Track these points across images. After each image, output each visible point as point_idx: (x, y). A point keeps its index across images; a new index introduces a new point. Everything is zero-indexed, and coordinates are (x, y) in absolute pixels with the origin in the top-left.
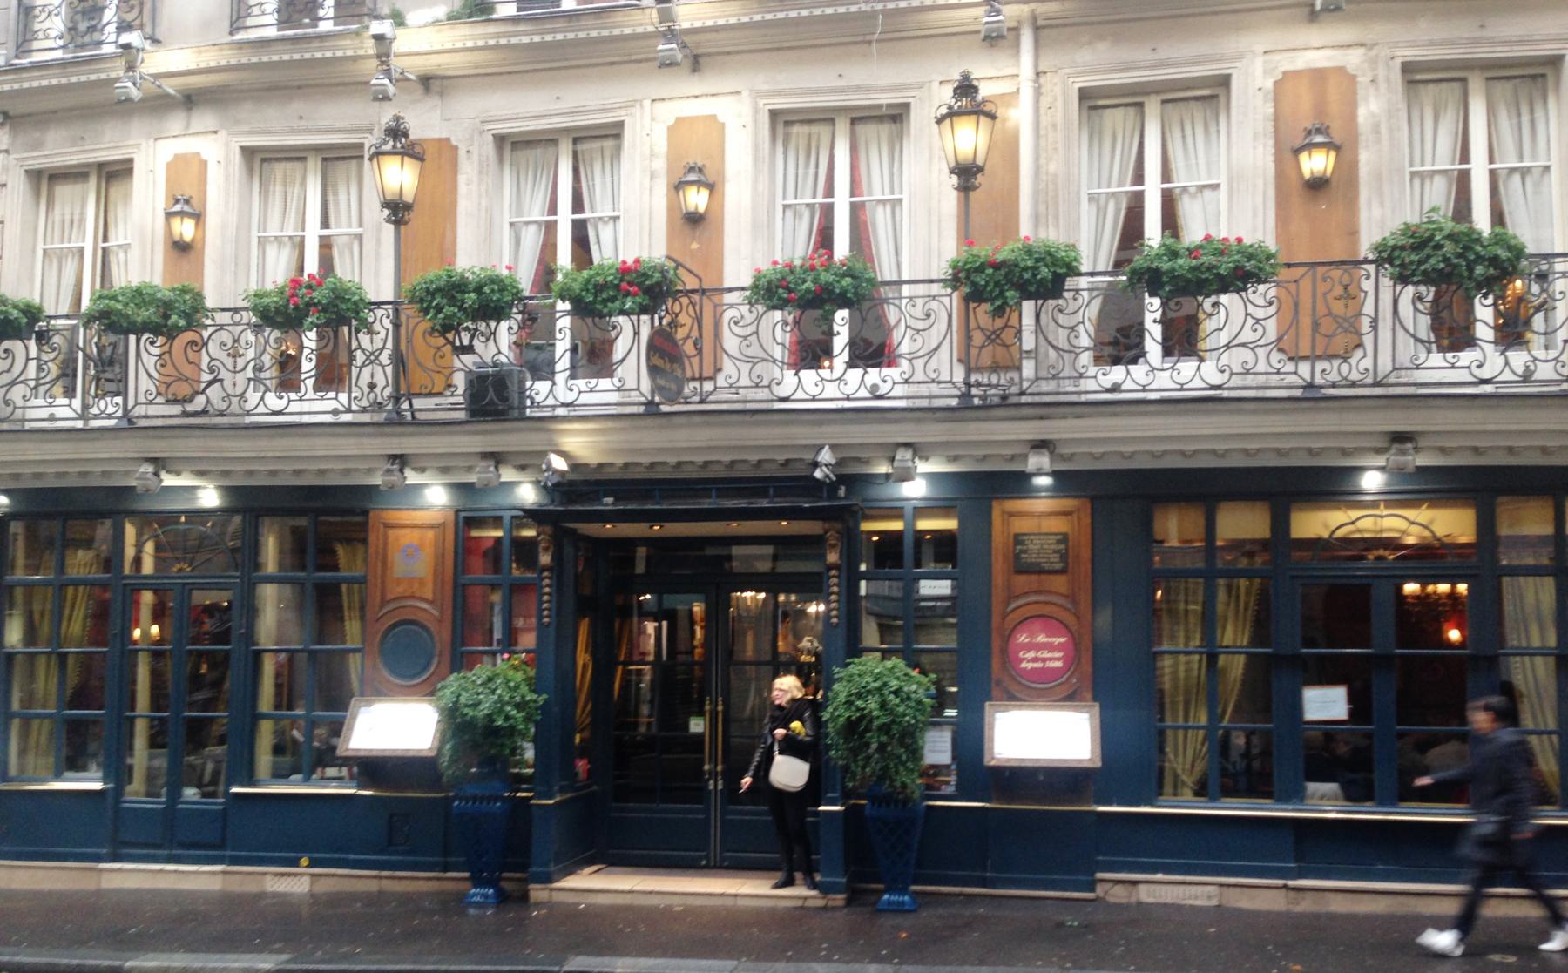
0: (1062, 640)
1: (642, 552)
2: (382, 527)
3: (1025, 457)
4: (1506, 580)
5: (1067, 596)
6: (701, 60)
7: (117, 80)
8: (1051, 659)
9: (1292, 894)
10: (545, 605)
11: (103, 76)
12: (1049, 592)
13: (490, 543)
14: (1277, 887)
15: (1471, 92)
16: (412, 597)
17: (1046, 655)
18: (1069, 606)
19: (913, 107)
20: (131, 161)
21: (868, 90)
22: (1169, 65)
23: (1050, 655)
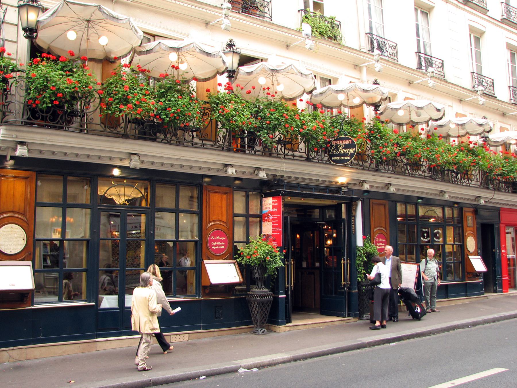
0: (224, 238)
2: (466, 274)
3: (15, 150)
7: (120, 113)
8: (221, 245)
10: (353, 226)
13: (449, 278)
15: (23, 209)
16: (219, 220)
17: (220, 244)
19: (339, 79)
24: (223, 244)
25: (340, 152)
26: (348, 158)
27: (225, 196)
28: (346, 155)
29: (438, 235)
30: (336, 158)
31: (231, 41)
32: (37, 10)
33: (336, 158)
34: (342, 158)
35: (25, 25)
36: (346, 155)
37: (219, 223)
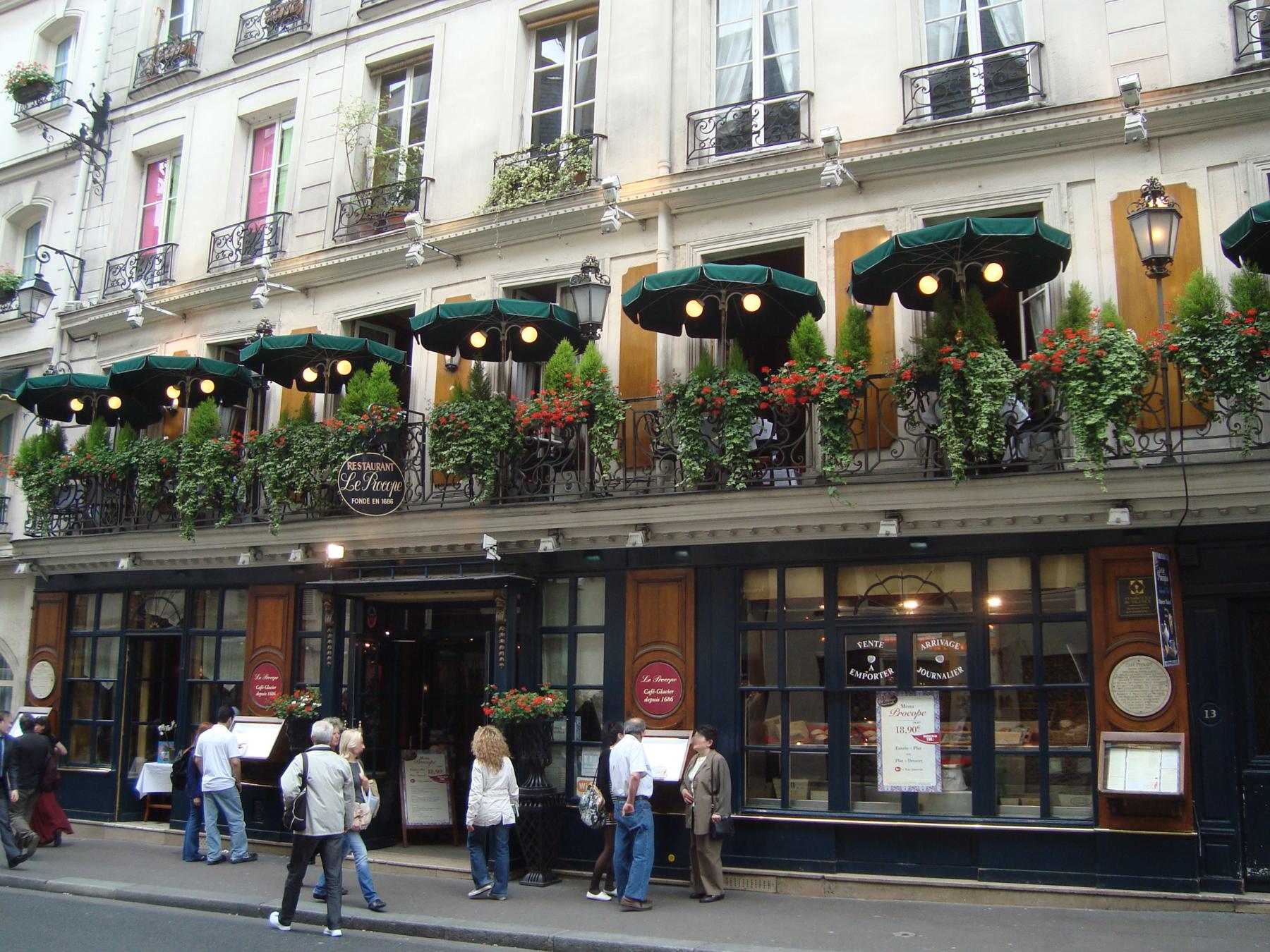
1: (429, 614)
3: (1106, 515)
4: (580, 636)
5: (677, 646)
6: (863, 185)
9: (827, 884)
11: (809, 167)
12: (664, 643)
14: (817, 879)
16: (270, 646)
18: (679, 654)
20: (1041, 204)
21: (1015, 195)
22: (760, 235)
23: (664, 692)
24: (274, 688)
25: (371, 486)
26: (391, 502)
27: (281, 601)
28: (385, 495)
29: (872, 659)
30: (361, 501)
31: (1153, 183)
32: (1168, 216)
33: (361, 501)
34: (376, 501)
35: (1146, 254)
36: (385, 495)
37: (271, 650)
